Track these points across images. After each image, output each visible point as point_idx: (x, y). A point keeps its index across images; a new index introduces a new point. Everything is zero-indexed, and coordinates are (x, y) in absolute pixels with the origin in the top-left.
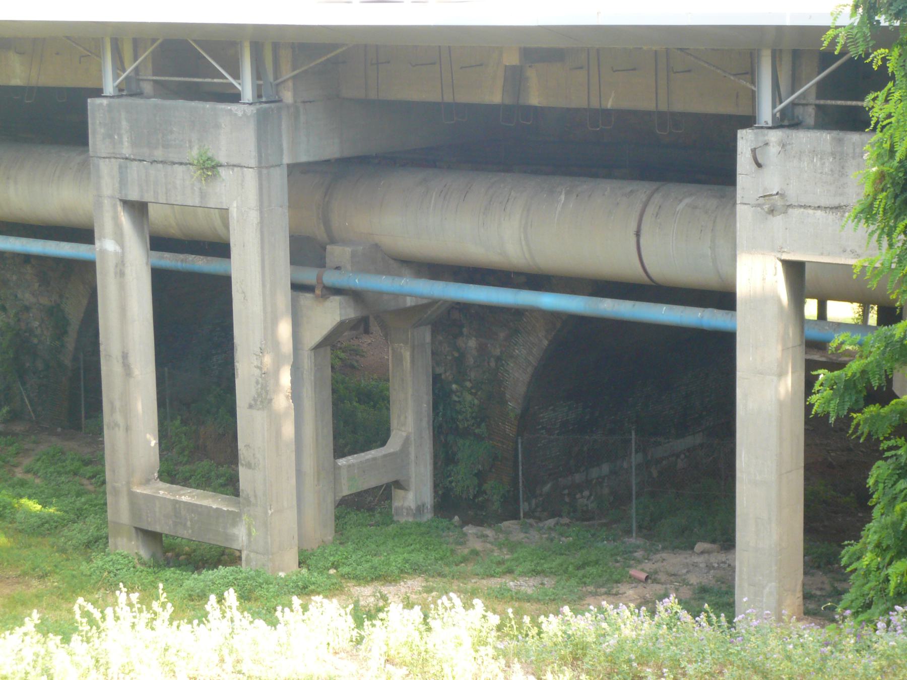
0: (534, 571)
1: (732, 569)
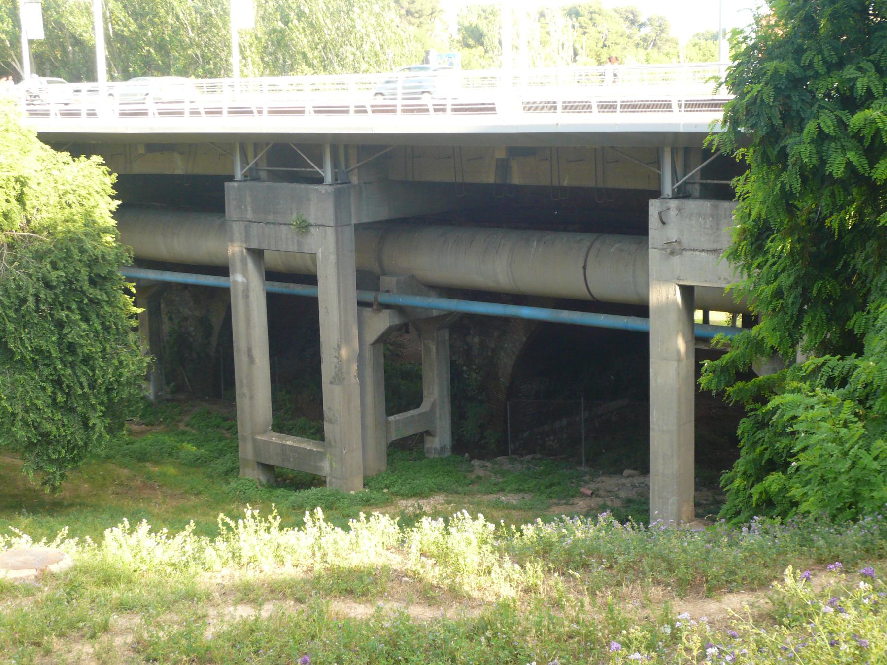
0: (518, 489)
1: (648, 487)
